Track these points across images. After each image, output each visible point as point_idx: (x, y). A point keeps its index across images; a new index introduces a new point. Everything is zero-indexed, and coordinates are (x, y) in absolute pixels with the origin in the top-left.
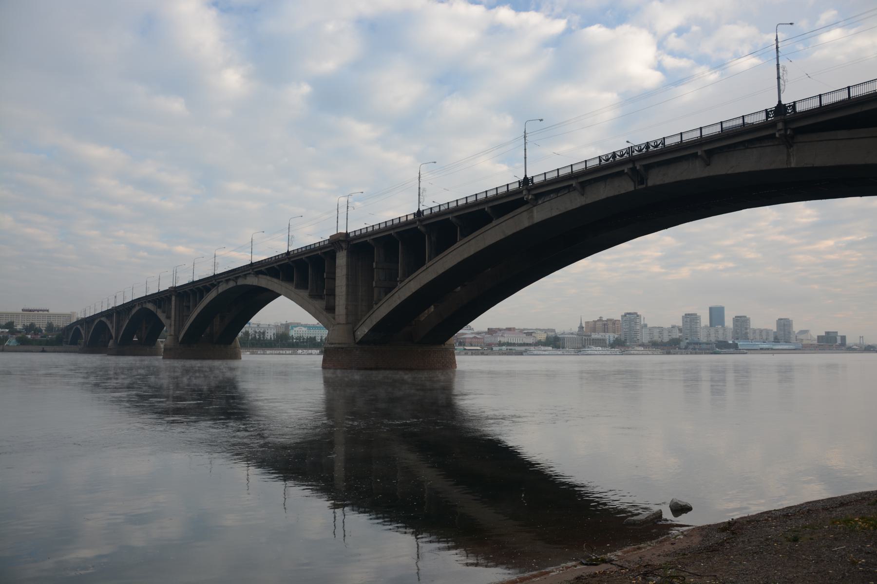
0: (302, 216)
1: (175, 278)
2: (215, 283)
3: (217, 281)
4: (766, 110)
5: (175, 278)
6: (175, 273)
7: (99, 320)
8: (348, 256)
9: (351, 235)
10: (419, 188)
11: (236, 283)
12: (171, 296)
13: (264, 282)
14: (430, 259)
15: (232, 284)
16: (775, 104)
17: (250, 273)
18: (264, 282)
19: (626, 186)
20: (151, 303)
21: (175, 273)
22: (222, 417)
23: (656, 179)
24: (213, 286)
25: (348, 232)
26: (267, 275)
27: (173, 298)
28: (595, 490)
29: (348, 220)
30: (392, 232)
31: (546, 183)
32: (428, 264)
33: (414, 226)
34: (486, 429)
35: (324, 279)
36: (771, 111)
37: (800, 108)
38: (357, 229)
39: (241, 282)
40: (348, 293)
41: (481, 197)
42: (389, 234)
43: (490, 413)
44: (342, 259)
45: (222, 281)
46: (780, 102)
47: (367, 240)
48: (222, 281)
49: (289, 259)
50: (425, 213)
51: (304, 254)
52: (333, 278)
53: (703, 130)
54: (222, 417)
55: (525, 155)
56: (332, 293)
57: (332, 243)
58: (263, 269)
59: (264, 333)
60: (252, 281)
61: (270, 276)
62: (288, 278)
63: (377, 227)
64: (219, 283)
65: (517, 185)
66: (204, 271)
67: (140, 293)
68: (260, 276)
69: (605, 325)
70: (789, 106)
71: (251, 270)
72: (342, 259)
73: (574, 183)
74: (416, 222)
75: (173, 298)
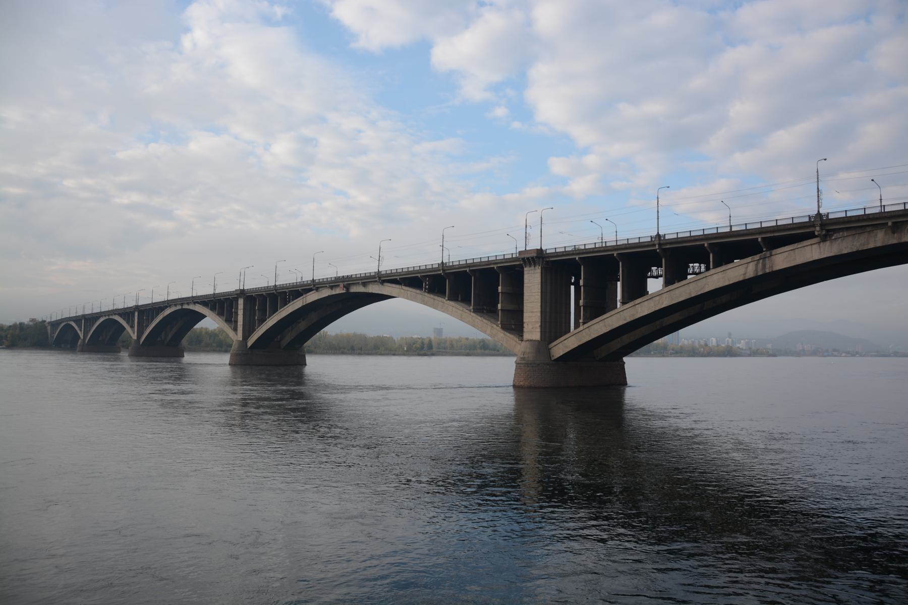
0: (668, 187)
1: (137, 300)
5: (137, 300)
6: (84, 308)
7: (66, 323)
9: (278, 286)
10: (526, 233)
12: (236, 299)
14: (281, 308)
15: (179, 307)
16: (816, 212)
17: (376, 281)
19: (339, 291)
21: (84, 308)
22: (891, 569)
23: (354, 289)
24: (166, 307)
25: (380, 270)
26: (401, 284)
27: (136, 314)
28: (864, 504)
29: (540, 235)
30: (230, 297)
31: (387, 275)
32: (279, 311)
33: (439, 272)
34: (319, 394)
35: (581, 286)
36: (812, 217)
38: (435, 263)
39: (186, 307)
43: (327, 380)
44: (241, 302)
46: (819, 211)
47: (494, 267)
49: (276, 290)
50: (316, 281)
51: (288, 288)
52: (236, 313)
54: (891, 569)
55: (658, 217)
56: (236, 322)
57: (523, 259)
58: (199, 301)
59: (706, 345)
61: (405, 285)
62: (213, 309)
64: (171, 305)
66: (160, 297)
67: (66, 315)
68: (197, 304)
69: (415, 341)
70: (825, 215)
72: (241, 302)
75: (136, 314)
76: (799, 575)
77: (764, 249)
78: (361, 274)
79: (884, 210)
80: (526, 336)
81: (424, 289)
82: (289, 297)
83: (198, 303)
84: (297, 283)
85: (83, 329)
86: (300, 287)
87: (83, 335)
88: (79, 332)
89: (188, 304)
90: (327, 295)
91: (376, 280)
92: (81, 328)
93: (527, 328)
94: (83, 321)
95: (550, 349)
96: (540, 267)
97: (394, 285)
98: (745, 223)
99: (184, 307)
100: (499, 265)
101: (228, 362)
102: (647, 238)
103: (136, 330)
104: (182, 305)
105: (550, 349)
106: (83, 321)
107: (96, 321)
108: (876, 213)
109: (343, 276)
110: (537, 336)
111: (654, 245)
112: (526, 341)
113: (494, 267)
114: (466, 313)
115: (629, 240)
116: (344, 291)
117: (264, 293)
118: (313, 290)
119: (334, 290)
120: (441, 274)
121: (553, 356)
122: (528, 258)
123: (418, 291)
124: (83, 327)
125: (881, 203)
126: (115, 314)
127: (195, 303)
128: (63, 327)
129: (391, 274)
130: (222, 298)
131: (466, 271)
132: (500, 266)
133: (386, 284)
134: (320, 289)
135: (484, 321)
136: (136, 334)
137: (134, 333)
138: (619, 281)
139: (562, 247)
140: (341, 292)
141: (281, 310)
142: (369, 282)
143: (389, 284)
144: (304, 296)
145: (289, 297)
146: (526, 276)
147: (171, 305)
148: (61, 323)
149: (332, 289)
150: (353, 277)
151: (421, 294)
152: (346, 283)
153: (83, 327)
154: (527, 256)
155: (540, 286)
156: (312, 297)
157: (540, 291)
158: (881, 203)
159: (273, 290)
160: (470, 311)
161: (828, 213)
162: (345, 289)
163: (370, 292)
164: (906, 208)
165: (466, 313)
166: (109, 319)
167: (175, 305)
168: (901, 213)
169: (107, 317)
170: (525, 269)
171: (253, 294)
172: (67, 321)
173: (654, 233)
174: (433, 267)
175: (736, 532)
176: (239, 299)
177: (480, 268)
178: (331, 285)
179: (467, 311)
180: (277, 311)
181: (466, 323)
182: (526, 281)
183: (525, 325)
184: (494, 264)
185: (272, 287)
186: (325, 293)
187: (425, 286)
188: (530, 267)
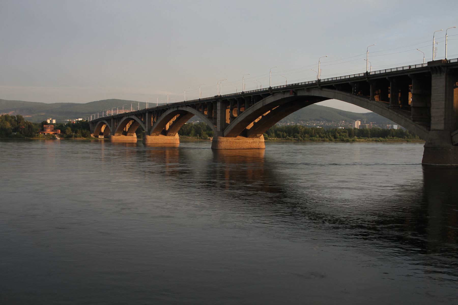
2: (168, 108)
3: (169, 107)
4: (364, 73)
7: (101, 121)
8: (221, 104)
11: (178, 109)
13: (189, 109)
17: (317, 87)
18: (189, 109)
19: (287, 95)
20: (134, 116)
23: (300, 94)
24: (167, 109)
27: (147, 114)
30: (189, 104)
31: (325, 83)
33: (365, 80)
34: (280, 171)
37: (451, 61)
40: (164, 119)
41: (303, 84)
42: (193, 104)
44: (219, 104)
45: (171, 107)
48: (171, 107)
51: (212, 100)
53: (376, 72)
56: (216, 118)
57: (431, 68)
60: (184, 109)
63: (279, 87)
64: (170, 108)
65: (241, 93)
68: (188, 107)
70: (448, 61)
71: (184, 104)
73: (305, 88)
74: (365, 78)
75: (147, 114)
76: (253, 185)
77: (337, 89)
78: (350, 75)
80: (433, 127)
81: (353, 92)
82: (253, 101)
83: (188, 106)
84: (261, 89)
85: (112, 126)
86: (261, 93)
87: (112, 129)
89: (182, 107)
90: (280, 98)
91: (317, 86)
92: (111, 125)
93: (434, 120)
94: (112, 120)
95: (452, 136)
96: (445, 74)
97: (330, 90)
98: (358, 73)
99: (179, 109)
100: (412, 73)
101: (211, 147)
102: (394, 69)
103: (147, 125)
104: (178, 107)
105: (452, 136)
106: (112, 120)
107: (120, 120)
108: (383, 73)
109: (292, 84)
110: (441, 126)
111: (365, 78)
112: (433, 130)
113: (348, 83)
114: (386, 109)
115: (329, 79)
116: (293, 95)
117: (228, 99)
118: (271, 95)
119: (285, 94)
120: (366, 81)
121: (454, 142)
122: (435, 67)
123: (348, 94)
126: (104, 120)
129: (328, 82)
132: (336, 85)
133: (324, 89)
134: (276, 94)
135: (400, 115)
136: (147, 128)
137: (146, 127)
138: (389, 93)
139: (352, 75)
140: (291, 96)
142: (298, 89)
143: (327, 90)
144: (264, 99)
145: (253, 101)
146: (433, 81)
147: (170, 108)
148: (98, 122)
149: (284, 94)
150: (299, 84)
151: (350, 96)
152: (294, 89)
154: (435, 65)
155: (444, 88)
156: (269, 100)
157: (444, 92)
159: (198, 102)
160: (389, 108)
161: (450, 60)
162: (293, 94)
163: (312, 95)
165: (386, 109)
167: (173, 108)
168: (384, 74)
169: (128, 117)
170: (433, 76)
171: (164, 108)
173: (365, 72)
174: (275, 88)
176: (218, 102)
177: (362, 80)
178: (283, 91)
179: (386, 108)
181: (386, 117)
182: (433, 85)
183: (432, 119)
184: (189, 103)
185: (241, 93)
186: (279, 97)
187: (354, 90)
188: (437, 74)
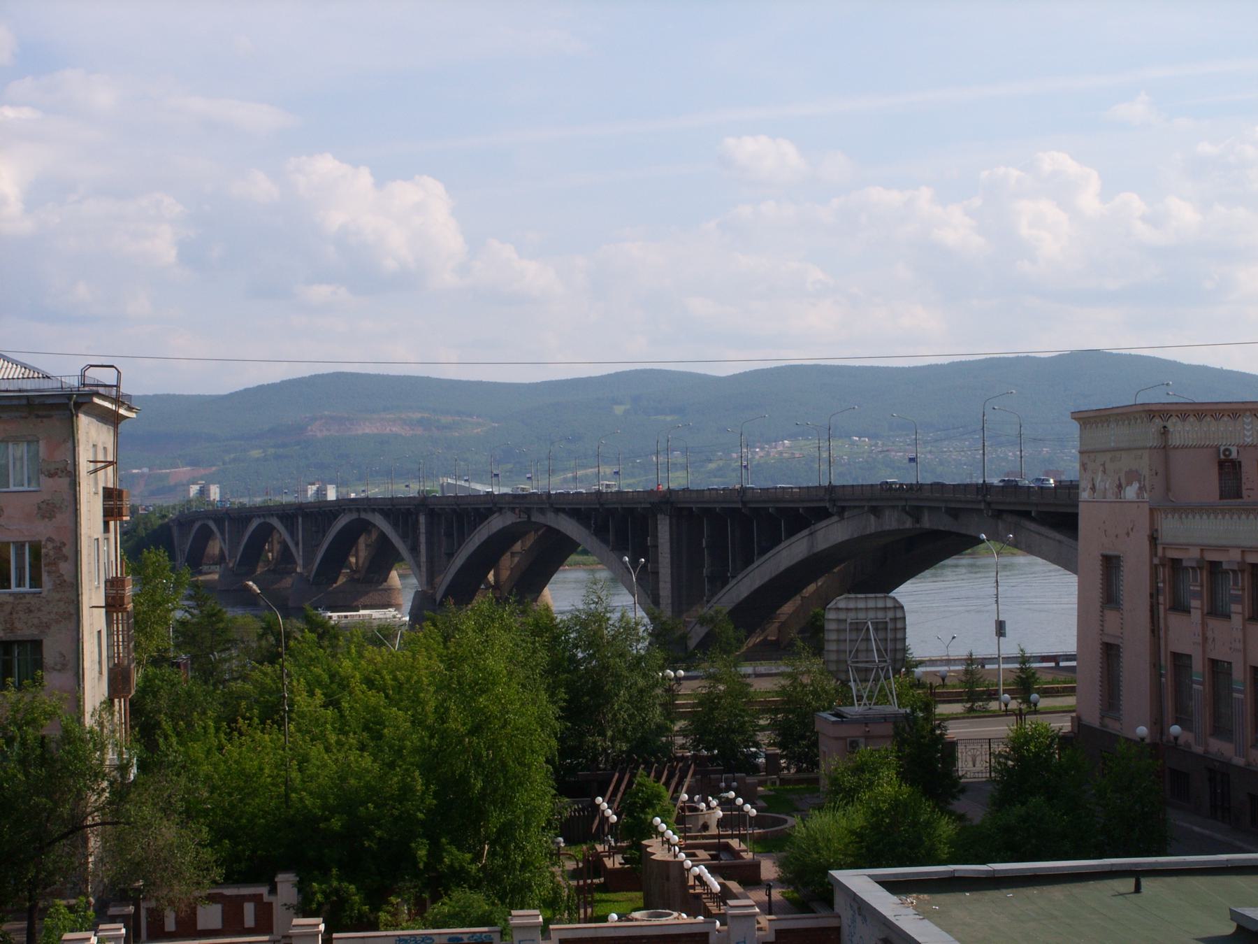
7: (262, 520)
27: (422, 519)
62: (600, 532)
79: (553, 930)
83: (563, 511)
88: (293, 549)
124: (423, 539)
125: (1235, 613)
127: (557, 511)
128: (198, 529)
130: (483, 506)
131: (692, 508)
141: (763, 559)
145: (475, 519)
153: (423, 539)
156: (832, 533)
158: (1235, 613)
164: (334, 942)
166: (265, 523)
172: (264, 516)
175: (1003, 487)
180: (753, 562)
